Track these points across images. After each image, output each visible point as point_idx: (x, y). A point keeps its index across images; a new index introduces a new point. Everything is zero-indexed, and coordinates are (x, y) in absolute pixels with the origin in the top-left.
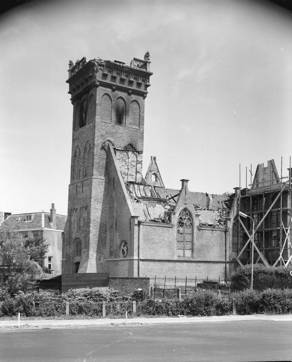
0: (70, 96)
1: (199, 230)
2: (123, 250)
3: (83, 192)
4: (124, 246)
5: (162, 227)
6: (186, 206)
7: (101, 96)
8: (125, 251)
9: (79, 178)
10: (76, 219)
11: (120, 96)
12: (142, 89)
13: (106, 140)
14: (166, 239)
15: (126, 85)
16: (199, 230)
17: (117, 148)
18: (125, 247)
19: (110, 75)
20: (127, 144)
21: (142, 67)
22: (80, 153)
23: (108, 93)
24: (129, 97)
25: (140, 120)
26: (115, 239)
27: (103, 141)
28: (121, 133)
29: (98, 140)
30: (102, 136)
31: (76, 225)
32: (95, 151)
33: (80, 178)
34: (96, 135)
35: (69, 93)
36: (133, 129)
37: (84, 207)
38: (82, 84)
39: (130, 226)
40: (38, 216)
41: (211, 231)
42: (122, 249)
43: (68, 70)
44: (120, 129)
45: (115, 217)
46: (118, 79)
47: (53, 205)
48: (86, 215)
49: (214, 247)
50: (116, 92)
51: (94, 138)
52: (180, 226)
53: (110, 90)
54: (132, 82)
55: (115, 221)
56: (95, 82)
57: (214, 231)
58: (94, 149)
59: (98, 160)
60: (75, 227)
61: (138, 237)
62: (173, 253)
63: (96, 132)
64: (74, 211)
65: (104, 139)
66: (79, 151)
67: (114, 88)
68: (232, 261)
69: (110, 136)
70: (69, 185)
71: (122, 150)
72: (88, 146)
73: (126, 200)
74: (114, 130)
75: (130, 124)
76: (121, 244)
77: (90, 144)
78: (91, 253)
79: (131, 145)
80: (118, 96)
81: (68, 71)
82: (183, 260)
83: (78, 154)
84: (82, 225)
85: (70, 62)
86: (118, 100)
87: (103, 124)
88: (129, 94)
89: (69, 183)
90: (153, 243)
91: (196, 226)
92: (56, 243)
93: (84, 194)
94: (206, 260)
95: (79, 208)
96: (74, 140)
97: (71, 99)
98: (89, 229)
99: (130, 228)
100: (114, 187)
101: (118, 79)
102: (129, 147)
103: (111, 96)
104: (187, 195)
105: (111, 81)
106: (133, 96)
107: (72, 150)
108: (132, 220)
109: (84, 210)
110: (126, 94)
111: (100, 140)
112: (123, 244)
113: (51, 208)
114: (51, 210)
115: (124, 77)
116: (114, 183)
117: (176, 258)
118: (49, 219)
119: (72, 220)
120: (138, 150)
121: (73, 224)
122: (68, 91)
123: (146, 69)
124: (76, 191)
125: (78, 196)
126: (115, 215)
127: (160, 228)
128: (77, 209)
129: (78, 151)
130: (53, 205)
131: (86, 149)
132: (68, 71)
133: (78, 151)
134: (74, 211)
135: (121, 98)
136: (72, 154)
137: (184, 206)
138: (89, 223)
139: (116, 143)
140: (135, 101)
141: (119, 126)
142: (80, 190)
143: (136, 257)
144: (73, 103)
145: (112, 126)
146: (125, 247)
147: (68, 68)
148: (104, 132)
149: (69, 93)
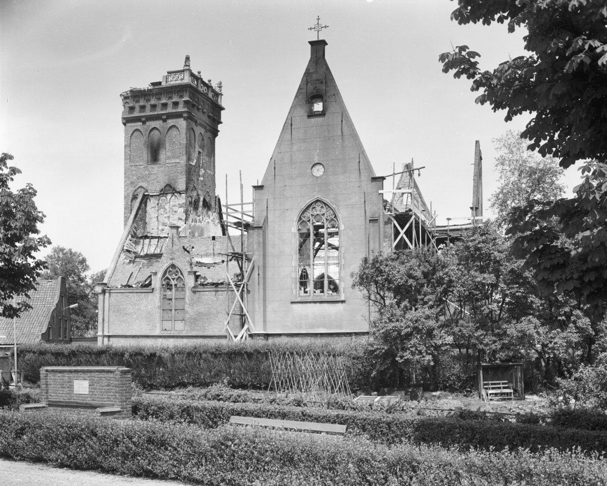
1: (194, 292)
5: (137, 293)
6: (174, 261)
7: (130, 135)
11: (153, 126)
13: (137, 187)
14: (143, 308)
15: (159, 111)
16: (194, 292)
17: (151, 194)
19: (137, 106)
20: (164, 185)
23: (138, 128)
27: (134, 189)
28: (156, 174)
36: (171, 165)
41: (214, 293)
44: (155, 168)
46: (148, 107)
49: (220, 315)
50: (148, 123)
52: (168, 289)
53: (140, 124)
57: (220, 292)
62: (153, 326)
65: (135, 187)
67: (164, 117)
69: (142, 181)
71: (158, 195)
74: (147, 172)
75: (169, 158)
78: (257, 306)
79: (168, 185)
80: (151, 128)
82: (168, 335)
86: (152, 133)
87: (133, 168)
88: (165, 121)
90: (125, 314)
94: (206, 334)
101: (148, 107)
102: (167, 188)
103: (142, 131)
104: (174, 247)
105: (173, 108)
110: (161, 122)
117: (157, 333)
120: (178, 190)
127: (135, 294)
135: (155, 128)
137: (170, 262)
139: (150, 188)
140: (173, 126)
141: (153, 166)
143: (100, 333)
145: (144, 167)
148: (135, 178)
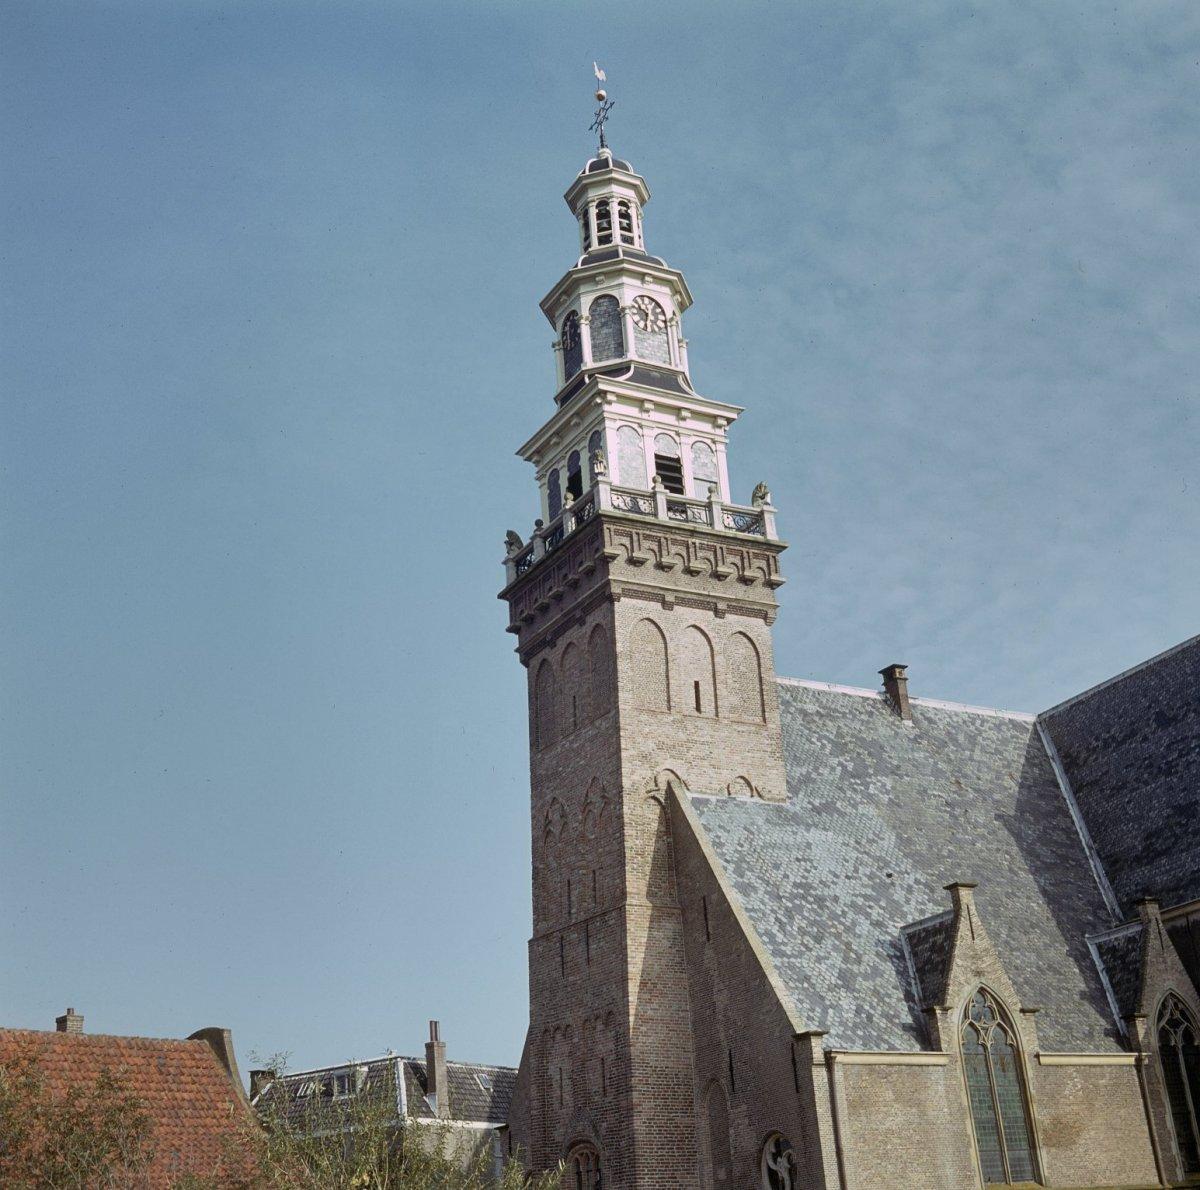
0: (514, 639)
2: (773, 1174)
3: (588, 960)
4: (775, 1156)
8: (784, 1175)
9: (570, 913)
10: (567, 1066)
12: (758, 594)
18: (783, 1161)
21: (747, 529)
22: (566, 823)
24: (721, 621)
25: (762, 695)
26: (732, 1131)
29: (633, 773)
30: (645, 757)
31: (567, 1089)
32: (626, 809)
33: (573, 911)
34: (624, 754)
35: (509, 630)
37: (597, 1018)
38: (559, 598)
39: (795, 1071)
40: (381, 1072)
42: (770, 1170)
43: (503, 559)
45: (724, 1044)
47: (434, 1025)
48: (611, 1046)
51: (619, 768)
54: (723, 576)
55: (728, 1059)
56: (608, 583)
58: (621, 803)
59: (637, 842)
60: (567, 1097)
61: (829, 1114)
63: (623, 746)
64: (558, 1036)
66: (561, 817)
68: (1184, 1185)
70: (530, 942)
72: (594, 798)
73: (764, 976)
76: (761, 1151)
77: (604, 789)
81: (505, 563)
83: (556, 830)
84: (595, 1089)
85: (510, 534)
88: (718, 613)
89: (531, 937)
91: (1029, 1055)
92: (1161, 1081)
93: (594, 969)
95: (580, 1023)
96: (537, 783)
97: (517, 651)
98: (629, 1099)
99: (796, 1081)
100: (708, 934)
104: (977, 941)
106: (730, 617)
107: (533, 817)
108: (799, 1047)
109: (600, 1027)
111: (639, 772)
112: (770, 1147)
113: (429, 1041)
114: (430, 1047)
115: (697, 562)
116: (706, 919)
118: (422, 1078)
119: (553, 1071)
121: (555, 1086)
122: (507, 624)
123: (764, 534)
124: (559, 959)
125: (571, 978)
126: (722, 1035)
128: (568, 1026)
129: (556, 817)
130: (434, 1025)
131: (591, 807)
132: (505, 563)
133: (556, 817)
134: (558, 1036)
136: (533, 829)
137: (976, 983)
138: (627, 1075)
142: (575, 953)
144: (525, 662)
146: (779, 1159)
147: (502, 552)
148: (651, 745)
149: (509, 630)
